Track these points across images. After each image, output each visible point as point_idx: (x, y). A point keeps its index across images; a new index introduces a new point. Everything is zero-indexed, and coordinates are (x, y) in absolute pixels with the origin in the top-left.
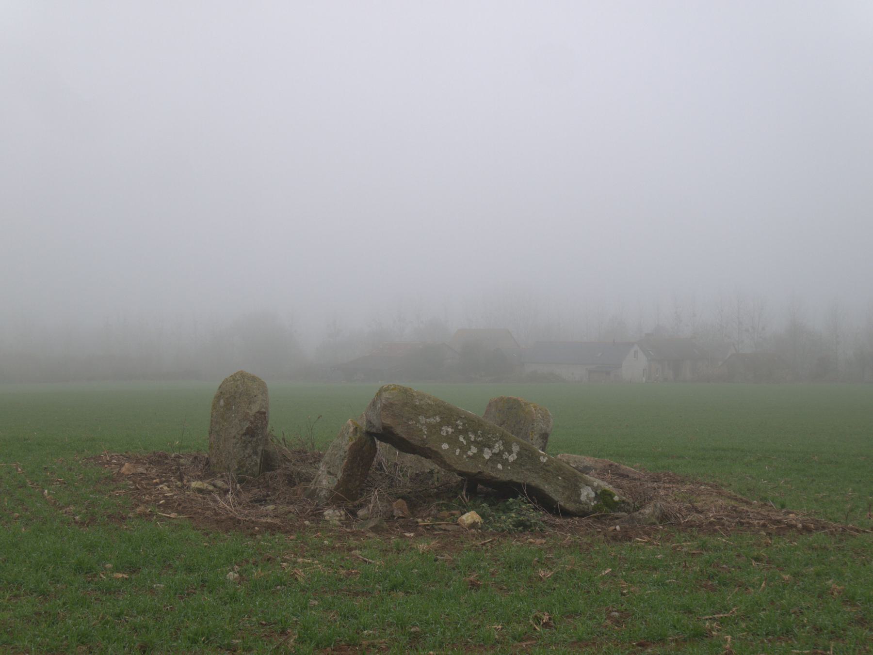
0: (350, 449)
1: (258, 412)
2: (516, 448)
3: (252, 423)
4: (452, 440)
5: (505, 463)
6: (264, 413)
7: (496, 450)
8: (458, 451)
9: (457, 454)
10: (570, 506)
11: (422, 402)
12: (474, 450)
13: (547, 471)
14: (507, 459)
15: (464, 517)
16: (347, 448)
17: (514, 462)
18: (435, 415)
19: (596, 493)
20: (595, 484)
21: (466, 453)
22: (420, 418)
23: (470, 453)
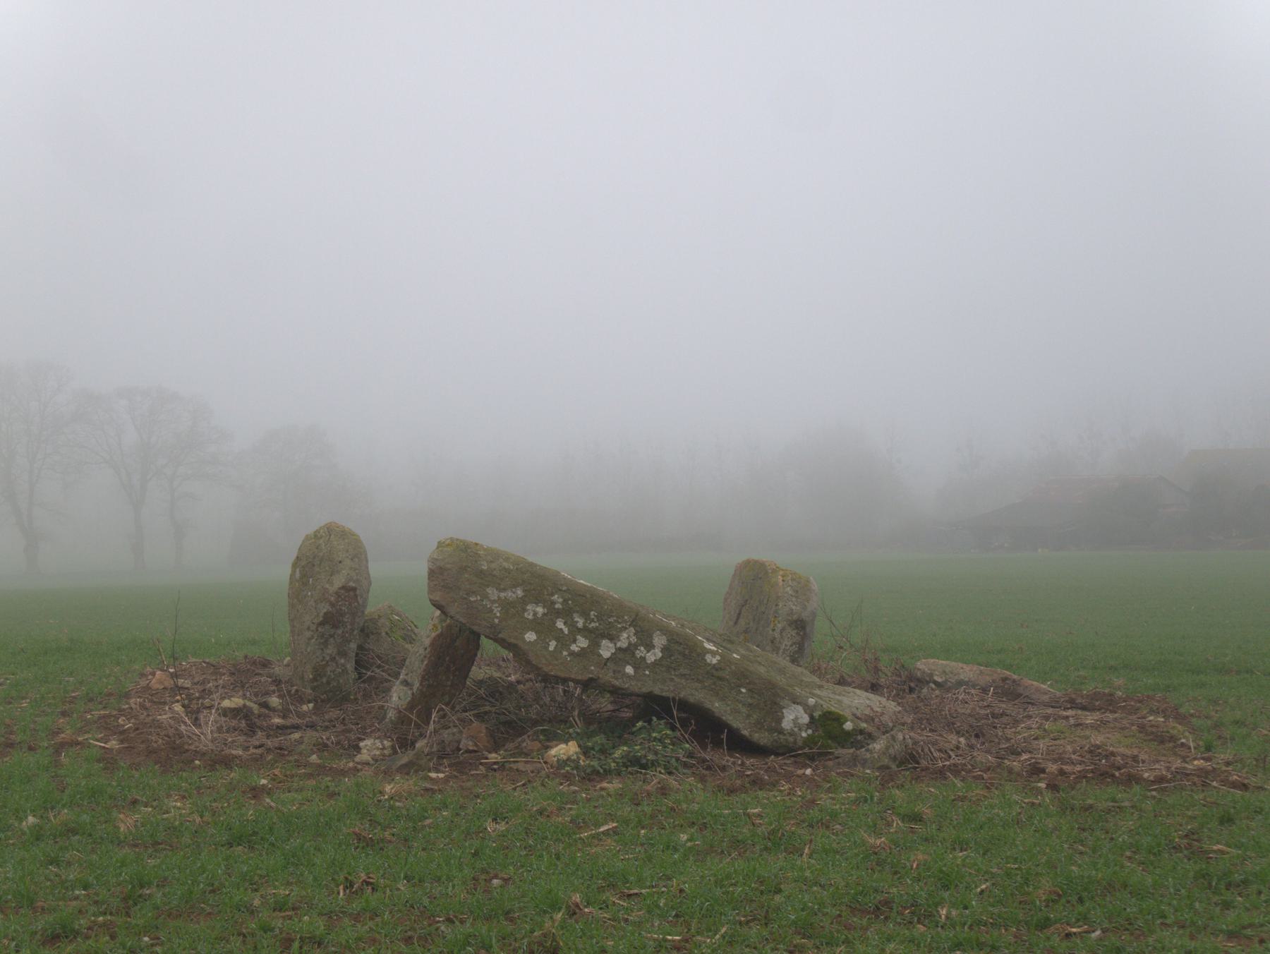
0: (432, 644)
1: (343, 588)
2: (659, 640)
3: (332, 605)
4: (544, 627)
5: (639, 664)
6: (354, 589)
7: (623, 643)
8: (552, 645)
9: (551, 648)
10: (761, 738)
11: (493, 566)
12: (582, 642)
13: (720, 679)
14: (644, 659)
15: (553, 752)
16: (427, 642)
17: (655, 664)
18: (515, 586)
19: (812, 717)
20: (812, 701)
21: (567, 647)
22: (489, 590)
23: (574, 648)
